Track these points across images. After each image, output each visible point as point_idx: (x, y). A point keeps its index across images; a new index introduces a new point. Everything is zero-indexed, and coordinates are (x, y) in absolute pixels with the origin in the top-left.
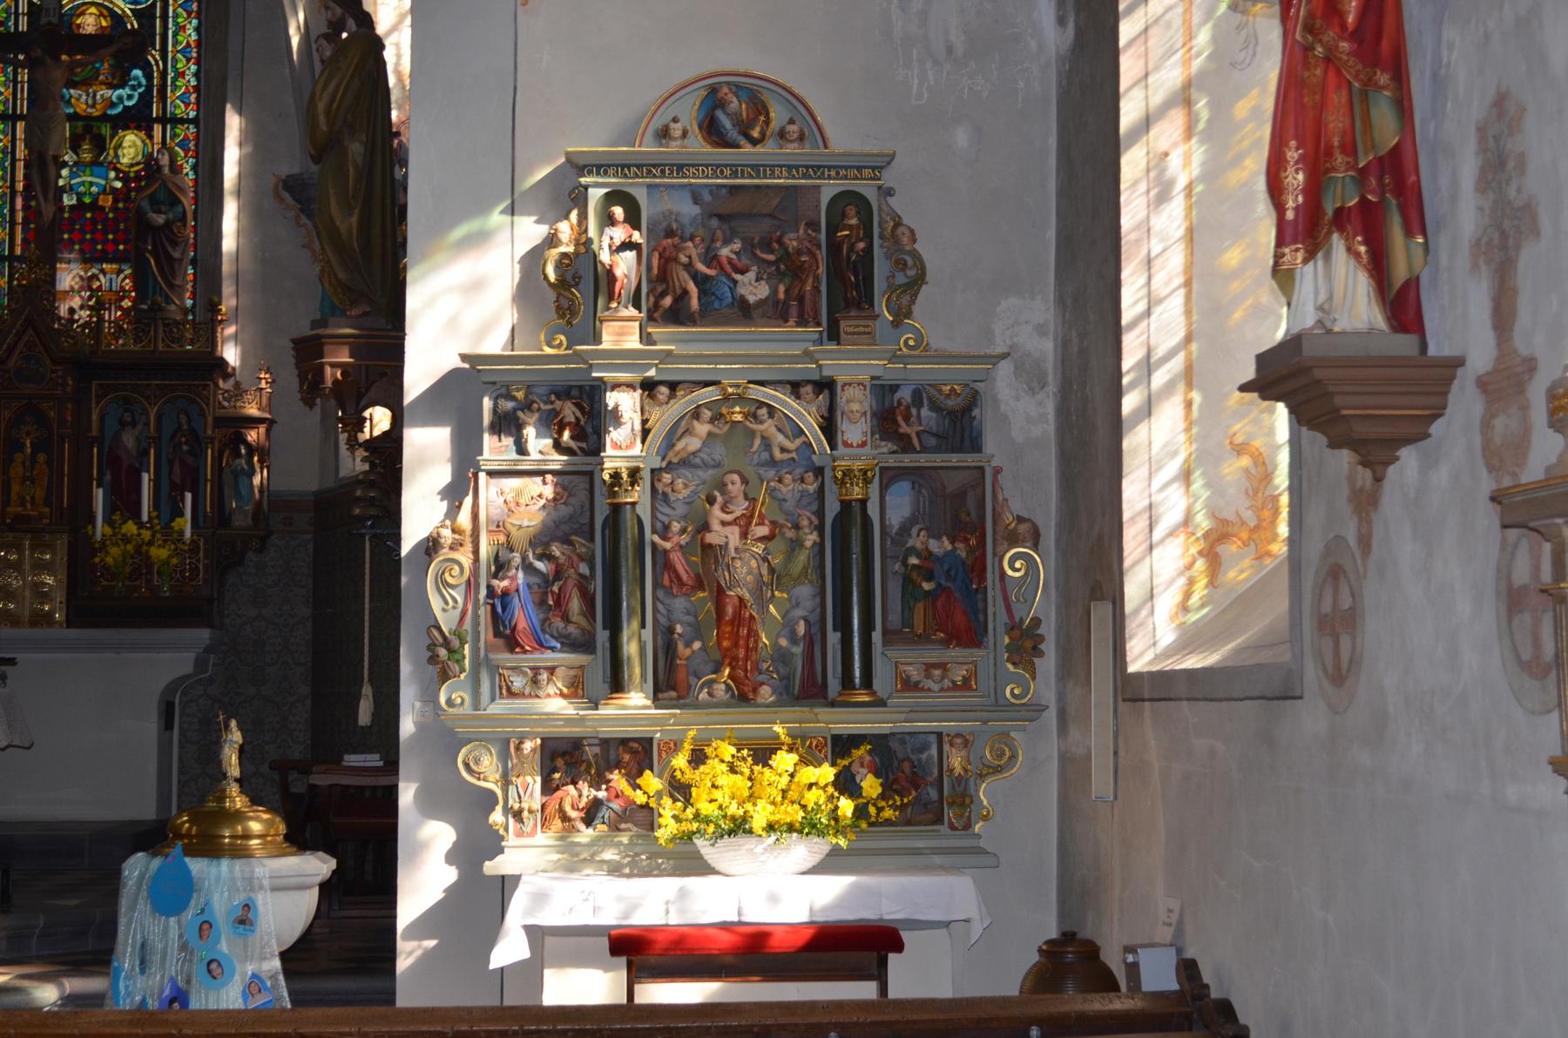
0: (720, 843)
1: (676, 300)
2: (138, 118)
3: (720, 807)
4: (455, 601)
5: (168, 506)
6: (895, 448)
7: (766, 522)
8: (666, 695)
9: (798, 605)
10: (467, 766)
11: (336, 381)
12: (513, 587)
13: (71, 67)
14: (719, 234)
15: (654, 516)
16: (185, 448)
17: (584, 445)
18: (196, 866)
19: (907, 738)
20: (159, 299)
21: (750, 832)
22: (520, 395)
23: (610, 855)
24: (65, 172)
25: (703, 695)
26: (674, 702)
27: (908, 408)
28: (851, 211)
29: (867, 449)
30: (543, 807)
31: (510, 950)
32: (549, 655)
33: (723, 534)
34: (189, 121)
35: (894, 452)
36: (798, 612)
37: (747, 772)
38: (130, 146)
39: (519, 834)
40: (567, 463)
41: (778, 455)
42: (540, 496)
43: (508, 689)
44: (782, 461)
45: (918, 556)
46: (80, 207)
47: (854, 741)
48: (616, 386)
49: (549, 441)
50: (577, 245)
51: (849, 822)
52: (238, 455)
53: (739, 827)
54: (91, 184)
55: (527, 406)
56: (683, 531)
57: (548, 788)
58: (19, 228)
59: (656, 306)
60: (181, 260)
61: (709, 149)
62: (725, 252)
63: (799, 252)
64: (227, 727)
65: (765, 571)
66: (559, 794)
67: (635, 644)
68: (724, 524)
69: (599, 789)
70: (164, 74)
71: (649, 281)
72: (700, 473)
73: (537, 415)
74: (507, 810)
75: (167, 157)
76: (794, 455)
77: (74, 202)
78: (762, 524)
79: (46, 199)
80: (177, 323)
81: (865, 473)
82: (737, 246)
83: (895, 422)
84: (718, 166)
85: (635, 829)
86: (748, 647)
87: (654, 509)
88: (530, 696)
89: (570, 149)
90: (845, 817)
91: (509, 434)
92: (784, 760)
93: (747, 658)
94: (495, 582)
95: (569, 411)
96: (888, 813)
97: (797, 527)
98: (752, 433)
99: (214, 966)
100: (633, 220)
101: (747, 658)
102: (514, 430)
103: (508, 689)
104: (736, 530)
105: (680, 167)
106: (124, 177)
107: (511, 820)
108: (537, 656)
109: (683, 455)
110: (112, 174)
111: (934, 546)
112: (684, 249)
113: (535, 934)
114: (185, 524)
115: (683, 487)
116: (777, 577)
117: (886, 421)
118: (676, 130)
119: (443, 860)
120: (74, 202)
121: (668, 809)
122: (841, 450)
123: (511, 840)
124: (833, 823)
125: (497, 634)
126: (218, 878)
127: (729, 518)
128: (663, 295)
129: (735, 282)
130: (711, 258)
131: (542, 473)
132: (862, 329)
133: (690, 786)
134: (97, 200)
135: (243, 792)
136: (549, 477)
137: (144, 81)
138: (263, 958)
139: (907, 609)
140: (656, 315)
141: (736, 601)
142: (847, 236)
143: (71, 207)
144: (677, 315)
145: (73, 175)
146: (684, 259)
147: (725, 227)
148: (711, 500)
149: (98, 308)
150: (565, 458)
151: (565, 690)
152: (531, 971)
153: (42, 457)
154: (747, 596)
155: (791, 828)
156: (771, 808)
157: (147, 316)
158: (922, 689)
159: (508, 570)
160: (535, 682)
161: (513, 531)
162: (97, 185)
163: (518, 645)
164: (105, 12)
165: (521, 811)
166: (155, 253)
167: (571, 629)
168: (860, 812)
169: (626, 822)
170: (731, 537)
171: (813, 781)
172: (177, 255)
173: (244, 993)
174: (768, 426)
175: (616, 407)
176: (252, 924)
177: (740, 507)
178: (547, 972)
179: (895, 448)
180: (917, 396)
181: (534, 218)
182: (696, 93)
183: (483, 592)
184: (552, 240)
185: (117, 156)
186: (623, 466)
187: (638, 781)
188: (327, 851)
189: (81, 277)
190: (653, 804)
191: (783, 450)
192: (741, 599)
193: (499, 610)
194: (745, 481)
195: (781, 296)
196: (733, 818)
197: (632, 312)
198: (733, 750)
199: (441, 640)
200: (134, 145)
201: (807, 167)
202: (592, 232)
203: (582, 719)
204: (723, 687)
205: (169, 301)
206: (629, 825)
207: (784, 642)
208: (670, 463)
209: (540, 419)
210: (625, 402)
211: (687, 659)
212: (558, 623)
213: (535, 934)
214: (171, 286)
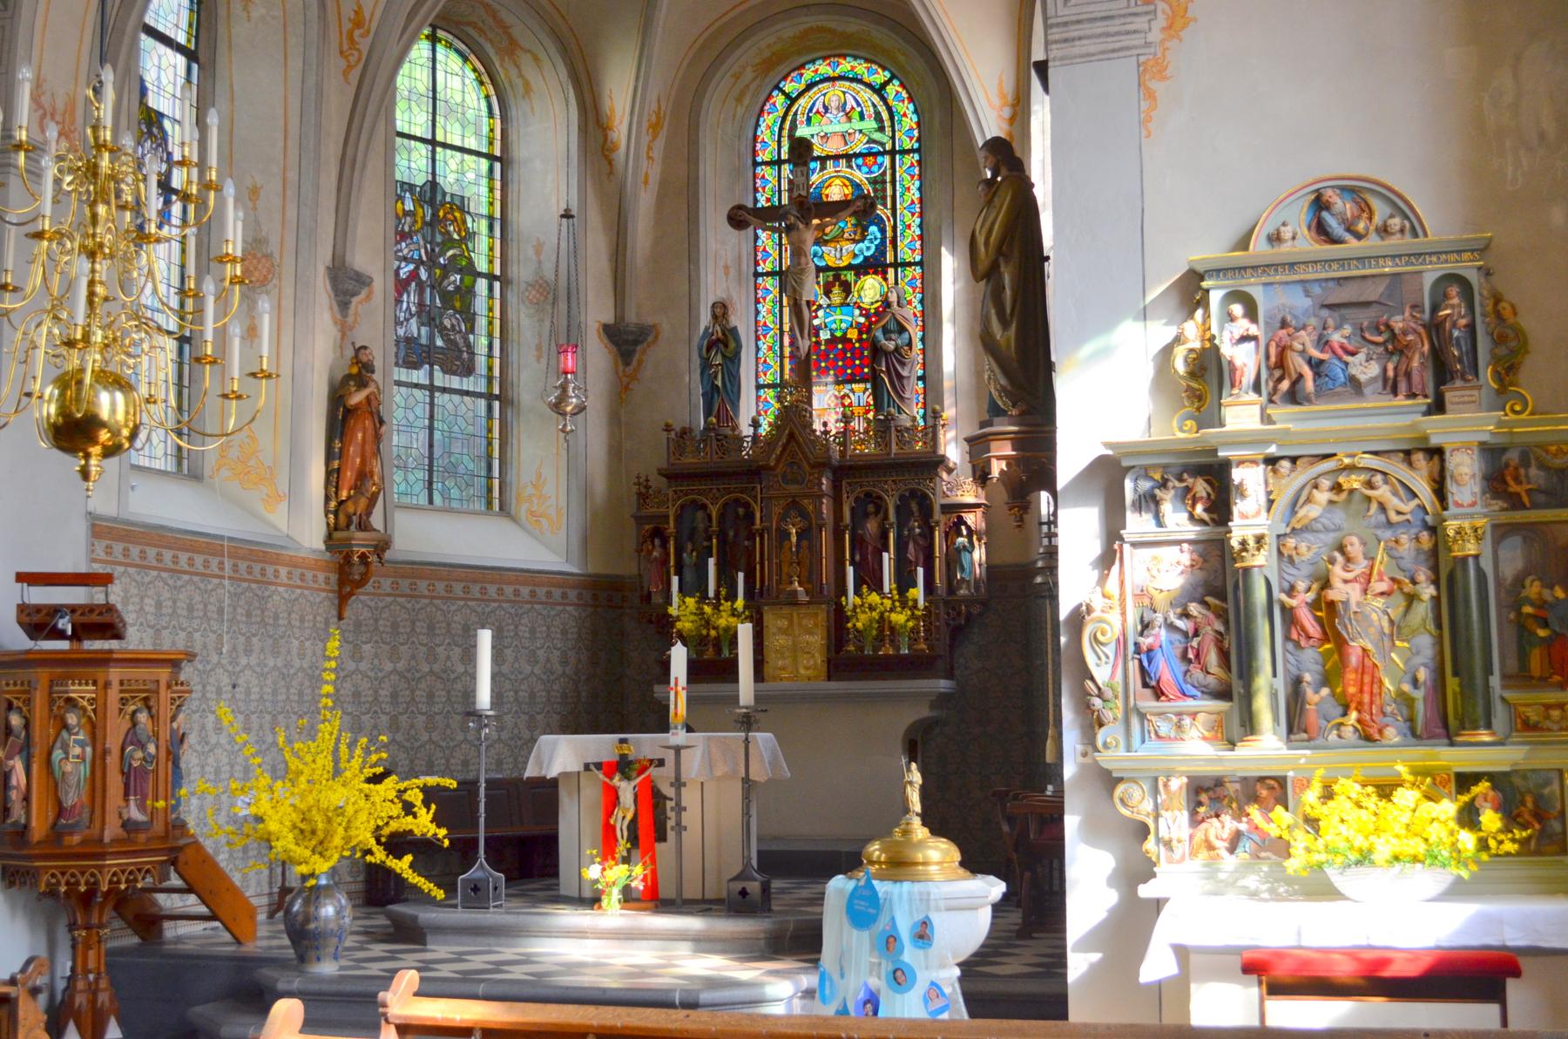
0: (1349, 872)
1: (1294, 384)
2: (874, 265)
3: (1348, 840)
4: (1107, 657)
5: (904, 581)
6: (1505, 505)
7: (1385, 578)
8: (1297, 737)
9: (1418, 653)
10: (1122, 800)
11: (1002, 472)
12: (1157, 644)
13: (821, 228)
14: (1330, 322)
15: (1281, 578)
16: (917, 531)
17: (1215, 516)
18: (881, 887)
19: (1529, 774)
20: (892, 410)
21: (1372, 862)
22: (1157, 476)
23: (1252, 881)
24: (821, 313)
25: (1333, 736)
26: (1306, 743)
27: (1516, 469)
28: (1454, 290)
29: (1478, 508)
30: (1191, 837)
31: (1157, 965)
32: (1190, 702)
33: (1343, 591)
34: (915, 264)
35: (1506, 510)
36: (1418, 660)
37: (1372, 807)
38: (870, 289)
39: (1170, 861)
40: (1198, 533)
41: (1394, 518)
42: (1178, 563)
43: (1156, 732)
44: (1398, 523)
45: (1532, 604)
46: (833, 341)
47: (1475, 778)
48: (1240, 463)
49: (1185, 515)
50: (1203, 341)
51: (1469, 854)
52: (960, 535)
53: (1364, 858)
54: (841, 321)
55: (1163, 484)
56: (1309, 590)
57: (1195, 821)
58: (787, 361)
59: (1275, 390)
60: (909, 377)
61: (1317, 247)
62: (1336, 338)
63: (1405, 333)
64: (909, 770)
65: (1385, 624)
66: (1204, 825)
67: (1267, 688)
68: (1346, 581)
69: (1240, 822)
70: (894, 228)
71: (1268, 367)
72: (1322, 536)
73: (1172, 492)
74: (1158, 840)
75: (895, 295)
76: (1408, 517)
77: (828, 337)
78: (1381, 580)
79: (802, 337)
80: (907, 429)
81: (1476, 531)
82: (1348, 330)
83: (1505, 482)
84: (1326, 261)
85: (1274, 857)
86: (1372, 693)
87: (1280, 570)
88: (1176, 739)
89: (1191, 258)
90: (1466, 850)
91: (1148, 510)
92: (1406, 797)
93: (1372, 703)
94: (1141, 640)
95: (1201, 487)
96: (1509, 847)
97: (1414, 582)
98: (1369, 499)
99: (899, 974)
100: (1251, 313)
101: (1372, 703)
102: (1152, 506)
103: (1156, 732)
104: (1357, 587)
105: (1292, 265)
106: (865, 313)
107: (1162, 848)
108: (1181, 703)
109: (1305, 521)
110: (857, 312)
111: (1546, 594)
112: (1298, 338)
113: (1182, 952)
114: (918, 593)
115: (1308, 549)
116: (1397, 629)
117: (1497, 481)
118: (1287, 233)
119: (1105, 883)
120: (828, 337)
121: (1300, 840)
122: (1453, 510)
123: (866, 935)
124: (1454, 855)
125: (1145, 685)
126: (900, 896)
127: (1349, 576)
128: (1280, 380)
129: (1347, 364)
130: (1323, 343)
131: (1178, 543)
132: (1466, 399)
133: (1317, 820)
134: (845, 334)
135: (924, 824)
136: (1185, 546)
137: (879, 235)
138: (943, 966)
139: (1523, 657)
140: (1274, 398)
141: (1360, 652)
142: (1448, 315)
143: (826, 341)
144: (1293, 397)
145: (827, 315)
146: (1299, 347)
147: (1336, 315)
148: (1332, 561)
149: (846, 419)
150: (1198, 528)
151: (1206, 734)
152: (1177, 988)
153: (805, 543)
154: (1369, 646)
155: (1415, 859)
156: (1395, 841)
157: (883, 428)
158: (1542, 729)
159: (1153, 628)
160: (1179, 727)
161: (1155, 594)
162: (845, 321)
163: (1163, 694)
164: (847, 183)
165: (1170, 841)
166: (888, 372)
167: (1210, 679)
168: (1483, 845)
169: (1265, 851)
170: (1352, 593)
171: (1434, 816)
172: (905, 373)
173: (925, 997)
174: (1383, 492)
175: (1241, 484)
176: (929, 939)
177: (1360, 567)
178: (1193, 987)
179: (1505, 505)
180: (1525, 460)
181: (1164, 321)
182: (1302, 200)
183: (1131, 648)
184: (1178, 340)
185: (860, 297)
186: (1250, 534)
187: (1271, 815)
188: (998, 876)
189: (836, 397)
190: (1286, 836)
191: (1399, 513)
192: (1364, 650)
193: (1145, 664)
194: (1364, 543)
195: (1391, 373)
196: (1361, 851)
197: (1253, 396)
198: (1358, 787)
199: (1096, 692)
200: (874, 287)
201: (1410, 255)
202: (1215, 330)
203: (1220, 760)
204: (1351, 729)
205: (900, 410)
206: (1269, 854)
207: (1407, 687)
208: (1294, 529)
209: (1176, 496)
210: (1250, 478)
211: (1316, 704)
212: (1197, 674)
213: (1182, 952)
214: (901, 398)
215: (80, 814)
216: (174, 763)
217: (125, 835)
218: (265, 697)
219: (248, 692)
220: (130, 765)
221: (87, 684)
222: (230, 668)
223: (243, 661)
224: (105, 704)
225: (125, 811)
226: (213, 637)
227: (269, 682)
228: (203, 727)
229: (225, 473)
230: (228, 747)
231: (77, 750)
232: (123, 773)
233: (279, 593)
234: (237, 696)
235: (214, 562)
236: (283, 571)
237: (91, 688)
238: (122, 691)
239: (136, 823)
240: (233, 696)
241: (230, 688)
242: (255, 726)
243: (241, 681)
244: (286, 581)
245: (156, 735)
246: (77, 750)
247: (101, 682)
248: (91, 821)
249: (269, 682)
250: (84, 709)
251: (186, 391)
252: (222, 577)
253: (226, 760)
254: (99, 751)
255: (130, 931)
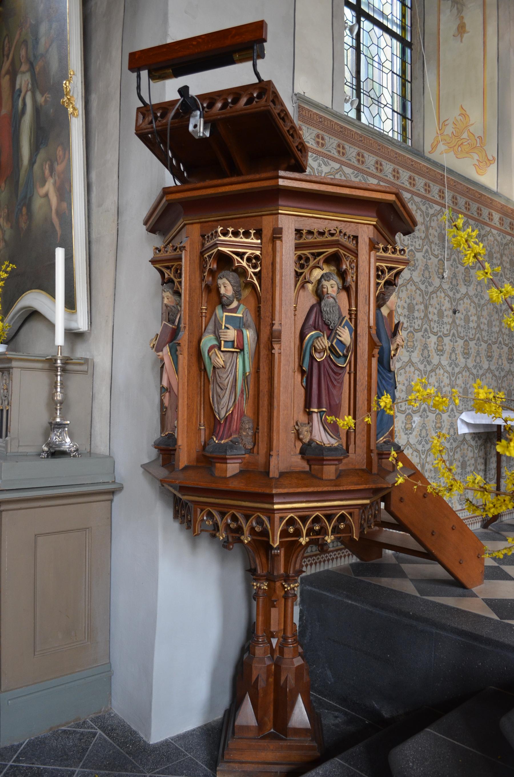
215: (239, 431)
216: (380, 361)
217: (304, 466)
218: (482, 326)
219: (467, 320)
220: (312, 358)
221: (247, 234)
222: (451, 294)
223: (463, 290)
224: (273, 264)
225: (304, 430)
226: (435, 261)
227: (485, 313)
228: (425, 347)
229: (442, 147)
230: (449, 369)
231: (231, 334)
232: (303, 372)
233: (493, 235)
234: (458, 322)
235: (435, 189)
236: (496, 216)
237: (254, 241)
238: (298, 247)
239: (321, 448)
240: (454, 321)
241: (451, 313)
242: (473, 352)
243: (461, 308)
244: (498, 225)
245: (354, 316)
246: (231, 334)
247: (267, 233)
248: (255, 443)
249: (485, 313)
250: (242, 272)
251: (408, 85)
252: (444, 206)
253: (446, 381)
254: (264, 336)
255: (347, 552)
